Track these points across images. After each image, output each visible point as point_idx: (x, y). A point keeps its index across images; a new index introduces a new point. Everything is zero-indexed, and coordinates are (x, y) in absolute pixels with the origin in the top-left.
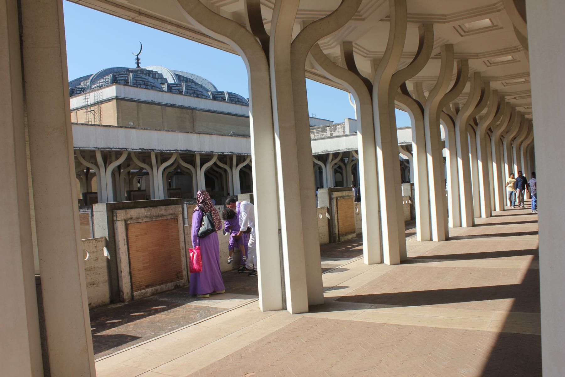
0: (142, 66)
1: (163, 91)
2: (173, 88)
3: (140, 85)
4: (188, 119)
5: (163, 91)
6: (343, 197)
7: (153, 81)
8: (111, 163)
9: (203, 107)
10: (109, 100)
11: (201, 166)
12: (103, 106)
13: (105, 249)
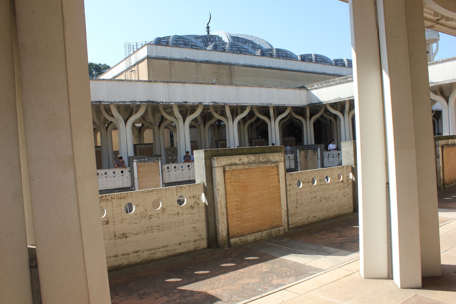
0: (211, 33)
1: (298, 60)
2: (219, 47)
3: (180, 45)
4: (226, 74)
6: (448, 145)
7: (195, 41)
8: (237, 115)
10: (143, 60)
11: (311, 116)
12: (140, 65)
13: (203, 195)
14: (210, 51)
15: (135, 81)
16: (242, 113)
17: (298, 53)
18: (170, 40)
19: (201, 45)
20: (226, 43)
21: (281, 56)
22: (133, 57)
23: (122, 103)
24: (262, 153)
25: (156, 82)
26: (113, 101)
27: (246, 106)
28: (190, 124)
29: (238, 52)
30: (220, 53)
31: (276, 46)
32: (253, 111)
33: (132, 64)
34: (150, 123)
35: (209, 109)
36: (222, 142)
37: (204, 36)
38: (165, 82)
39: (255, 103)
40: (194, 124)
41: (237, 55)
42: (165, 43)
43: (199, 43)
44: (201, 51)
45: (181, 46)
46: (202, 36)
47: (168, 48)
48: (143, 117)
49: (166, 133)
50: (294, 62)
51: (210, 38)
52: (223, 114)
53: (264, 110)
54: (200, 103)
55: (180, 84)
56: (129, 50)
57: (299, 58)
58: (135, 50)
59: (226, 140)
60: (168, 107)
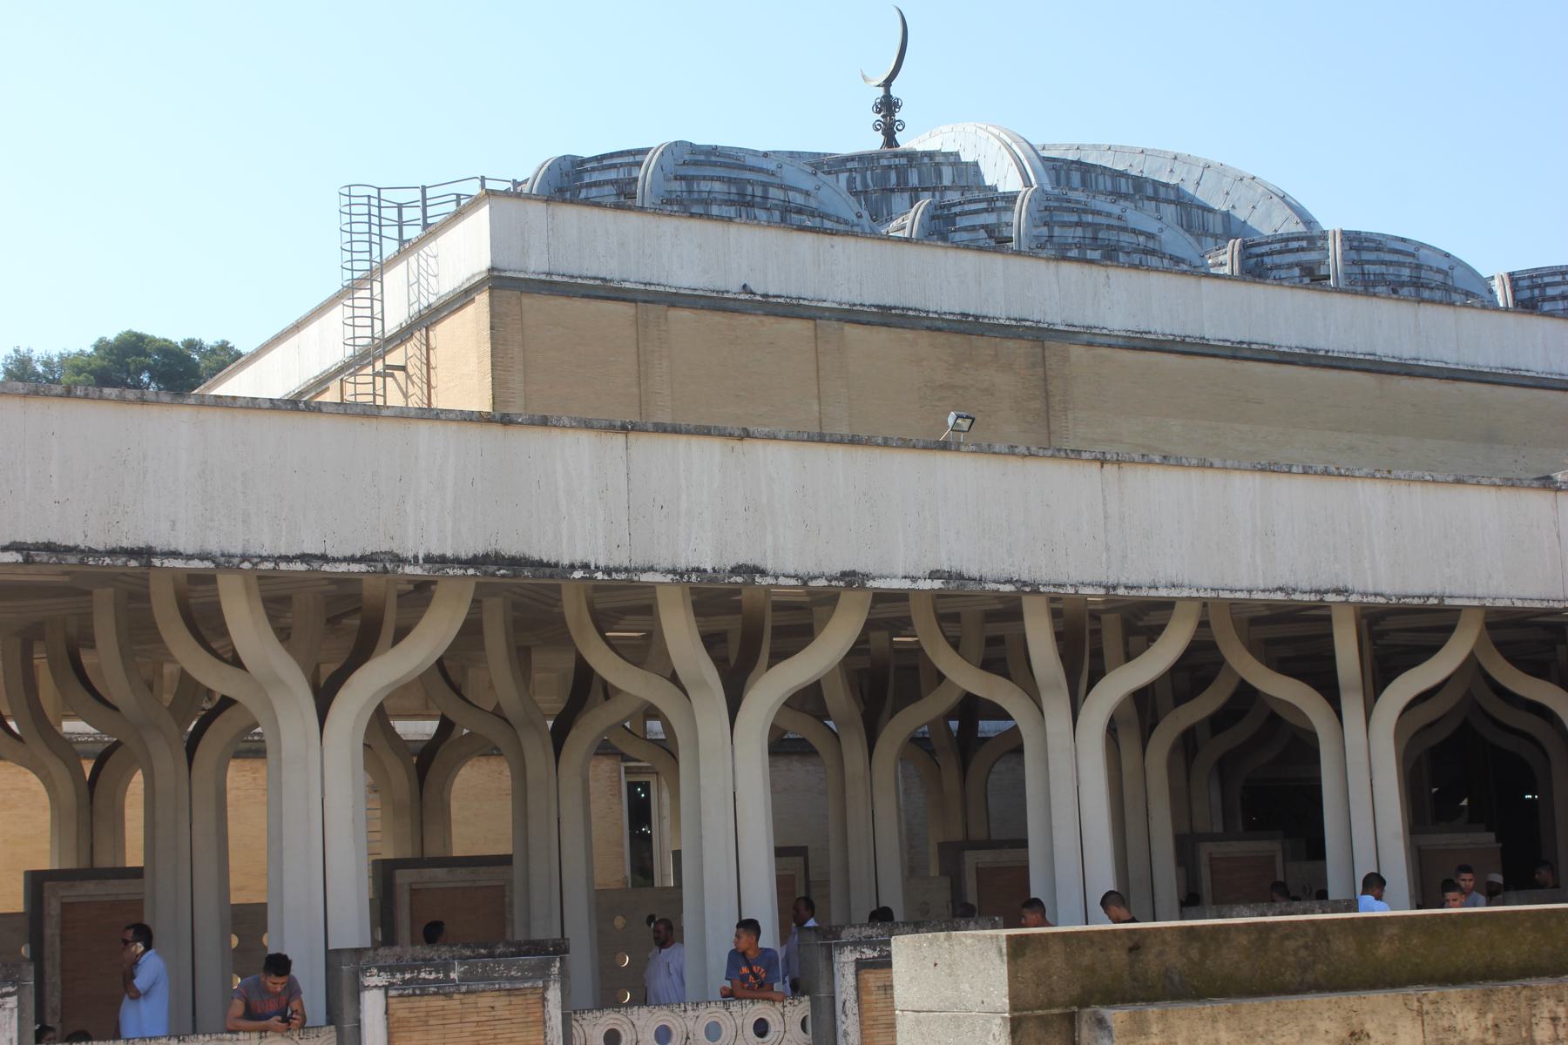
0: (908, 141)
1: (1497, 308)
2: (962, 222)
3: (707, 203)
4: (1021, 388)
5: (1497, 308)
8: (1097, 675)
9: (1118, 320)
10: (462, 298)
12: (443, 333)
14: (907, 247)
15: (402, 415)
16: (1129, 657)
17: (1494, 258)
18: (645, 174)
19: (847, 207)
20: (1011, 198)
21: (1381, 279)
22: (395, 279)
23: (299, 567)
24: (1540, 972)
25: (544, 422)
26: (237, 549)
27: (1168, 605)
28: (774, 728)
29: (1096, 255)
30: (970, 258)
31: (1337, 215)
32: (1212, 646)
33: (393, 323)
34: (498, 713)
35: (903, 624)
36: (987, 857)
37: (865, 160)
38: (611, 428)
39: (1229, 582)
40: (801, 727)
41: (1086, 269)
42: (608, 189)
43: (835, 196)
44: (851, 241)
45: (715, 210)
46: (851, 158)
47: (631, 221)
48: (447, 673)
49: (606, 790)
50: (1470, 321)
51: (902, 172)
52: (1002, 653)
53: (1292, 634)
54: (851, 579)
55: (714, 445)
56: (375, 236)
57: (1502, 295)
58: (412, 232)
59: (1023, 843)
60: (623, 605)
